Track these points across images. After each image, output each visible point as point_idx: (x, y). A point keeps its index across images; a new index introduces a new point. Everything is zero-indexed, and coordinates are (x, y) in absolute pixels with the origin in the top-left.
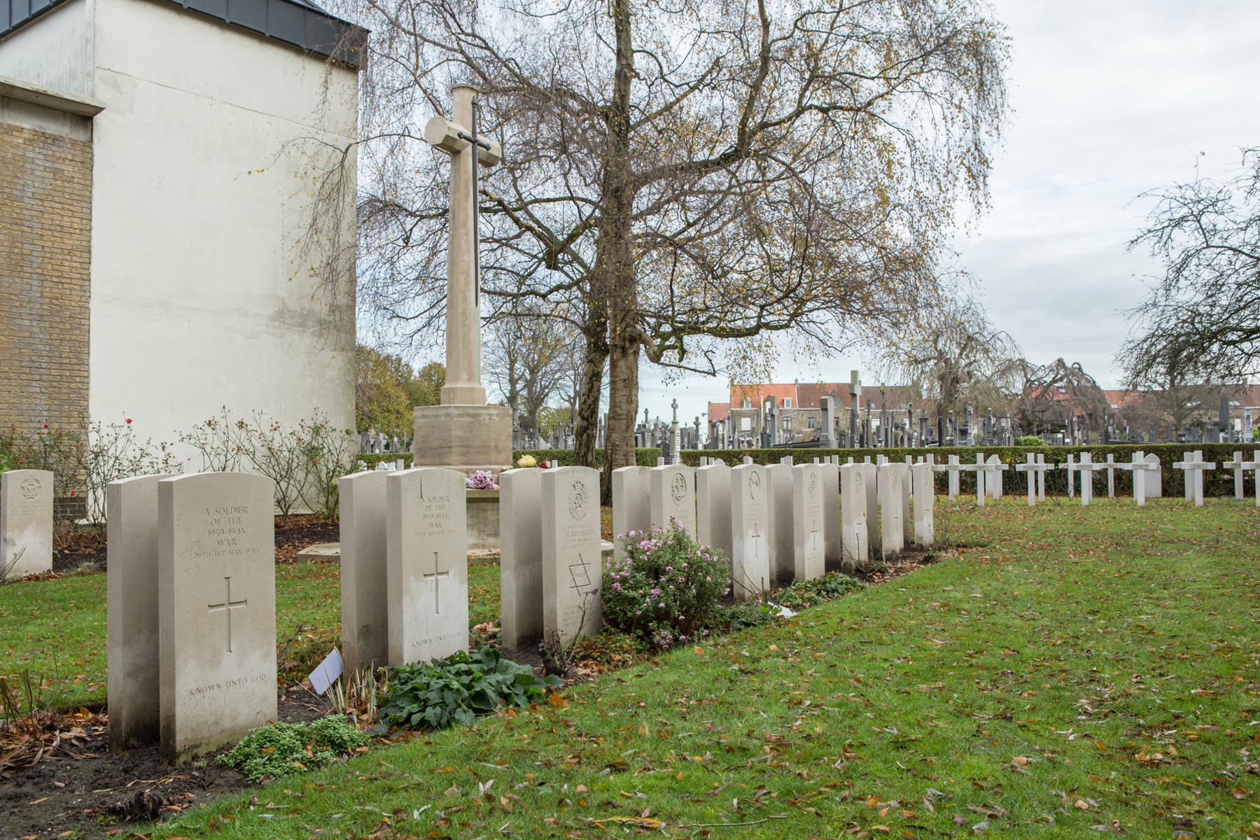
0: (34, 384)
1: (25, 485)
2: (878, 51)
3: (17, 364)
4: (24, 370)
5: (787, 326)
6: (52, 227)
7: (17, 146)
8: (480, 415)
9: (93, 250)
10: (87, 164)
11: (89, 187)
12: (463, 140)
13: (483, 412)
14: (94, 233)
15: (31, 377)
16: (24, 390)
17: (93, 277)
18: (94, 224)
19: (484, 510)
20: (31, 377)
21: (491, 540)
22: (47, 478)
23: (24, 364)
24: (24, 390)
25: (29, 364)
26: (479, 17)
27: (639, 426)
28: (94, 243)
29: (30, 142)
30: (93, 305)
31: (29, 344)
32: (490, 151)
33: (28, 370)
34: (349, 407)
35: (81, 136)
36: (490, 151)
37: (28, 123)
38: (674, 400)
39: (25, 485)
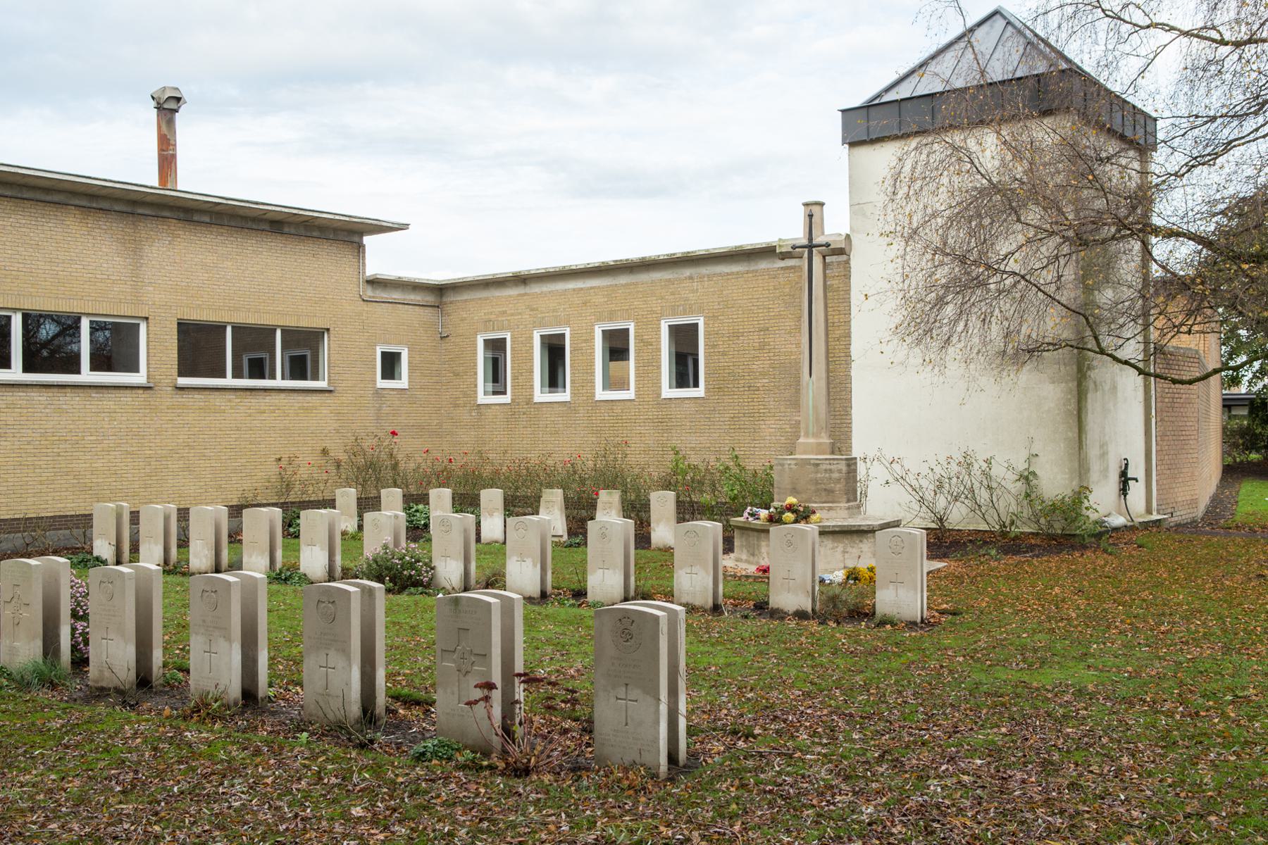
10: (847, 276)
12: (797, 250)
28: (853, 330)
34: (1070, 434)
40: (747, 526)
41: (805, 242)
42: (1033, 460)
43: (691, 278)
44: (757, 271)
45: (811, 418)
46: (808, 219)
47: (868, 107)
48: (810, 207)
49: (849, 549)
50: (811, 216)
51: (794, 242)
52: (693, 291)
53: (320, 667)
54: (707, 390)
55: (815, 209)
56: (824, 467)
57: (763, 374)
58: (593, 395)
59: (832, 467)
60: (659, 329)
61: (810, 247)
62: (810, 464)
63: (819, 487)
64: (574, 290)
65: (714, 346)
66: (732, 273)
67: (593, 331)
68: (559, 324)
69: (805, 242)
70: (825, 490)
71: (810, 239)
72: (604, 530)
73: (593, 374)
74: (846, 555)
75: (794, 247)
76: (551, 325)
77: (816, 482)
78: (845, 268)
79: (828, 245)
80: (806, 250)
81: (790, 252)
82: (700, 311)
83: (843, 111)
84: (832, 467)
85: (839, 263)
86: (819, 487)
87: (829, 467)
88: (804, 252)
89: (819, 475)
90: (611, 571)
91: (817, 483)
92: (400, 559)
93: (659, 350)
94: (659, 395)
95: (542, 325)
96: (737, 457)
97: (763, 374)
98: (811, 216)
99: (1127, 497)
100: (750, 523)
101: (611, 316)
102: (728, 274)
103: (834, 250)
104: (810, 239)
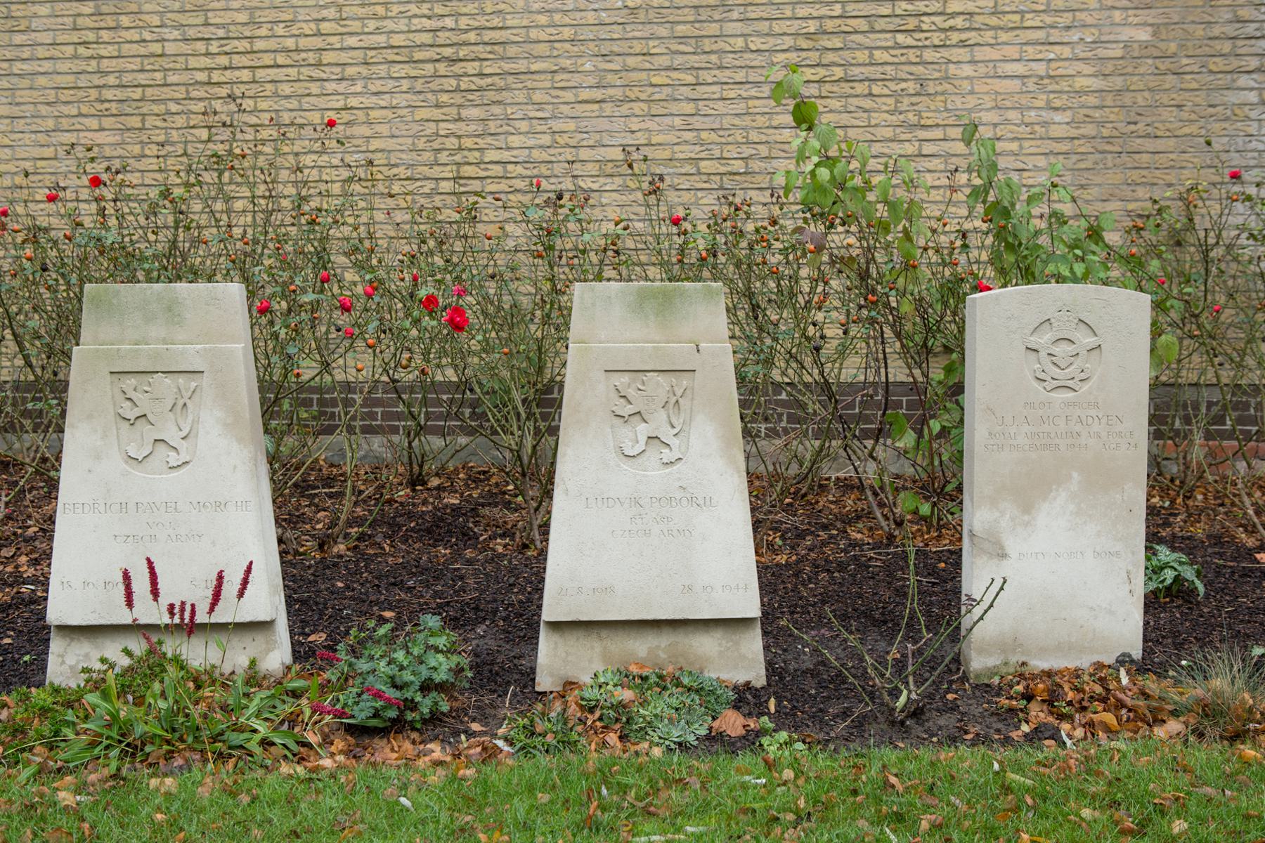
0: (1243, 81)
1: (1043, 340)
2: (227, 277)
3: (1200, 31)
4: (1218, 45)
5: (900, 156)
6: (458, 99)
15: (1235, 63)
16: (1216, 98)
20: (1235, 63)
22: (236, 290)
23: (1216, 31)
24: (1216, 98)
25: (1230, 30)
26: (387, 752)
33: (1226, 47)
38: (251, 563)
39: (1043, 340)
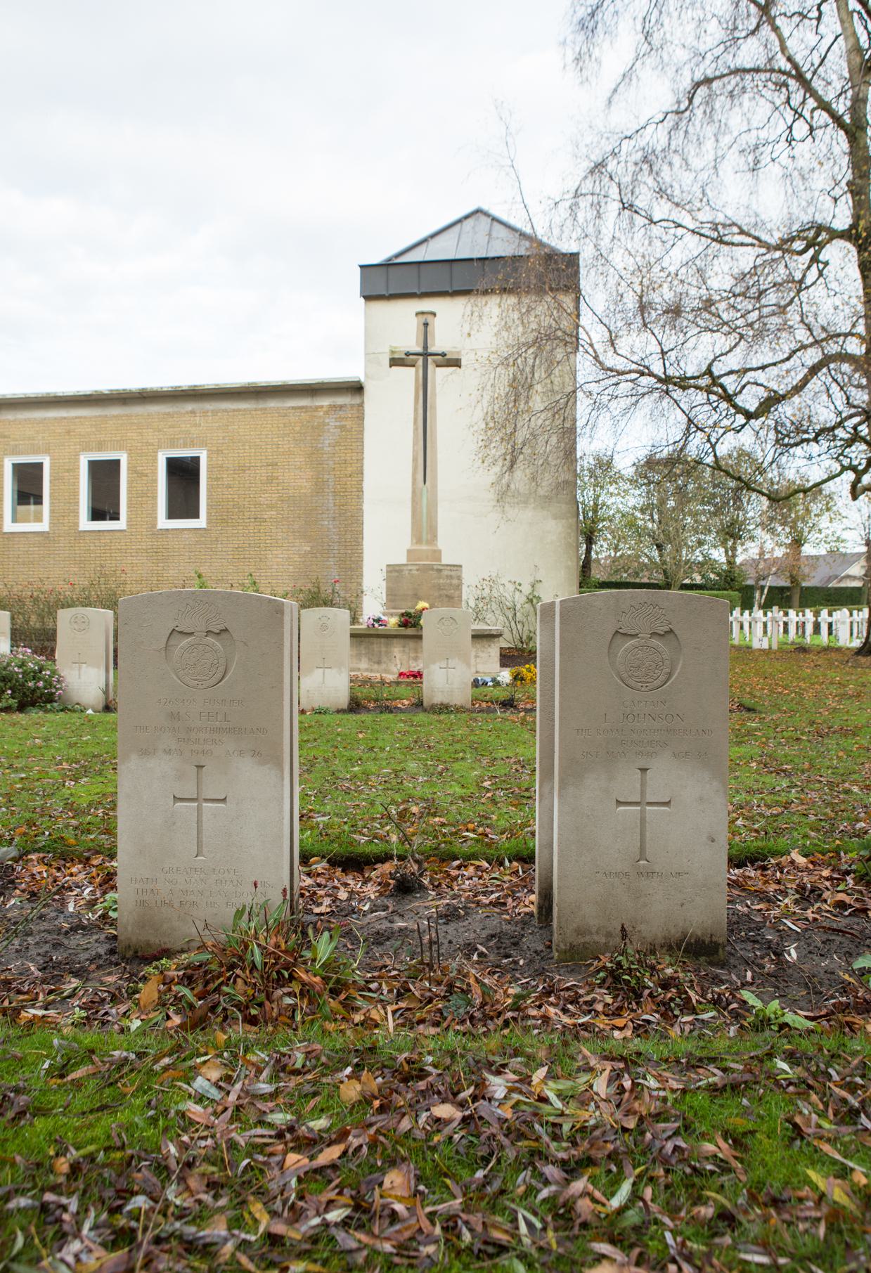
7: (320, 417)
8: (402, 571)
9: (365, 472)
10: (360, 418)
11: (361, 432)
12: (411, 357)
13: (405, 568)
14: (365, 462)
17: (364, 490)
18: (365, 455)
19: (373, 643)
21: (376, 666)
27: (394, 572)
28: (365, 467)
29: (327, 413)
30: (365, 507)
31: (327, 536)
32: (447, 357)
34: (570, 563)
35: (357, 400)
36: (447, 357)
37: (325, 402)
40: (371, 632)
41: (431, 350)
42: (538, 585)
43: (193, 412)
44: (266, 409)
45: (425, 524)
46: (422, 327)
47: (387, 265)
48: (425, 316)
49: (481, 654)
50: (426, 325)
51: (408, 349)
52: (195, 425)
53: (176, 799)
54: (209, 520)
55: (430, 318)
56: (446, 573)
57: (271, 507)
58: (77, 524)
59: (453, 573)
60: (155, 460)
61: (426, 354)
62: (433, 569)
63: (441, 592)
64: (56, 419)
65: (217, 479)
66: (239, 410)
67: (77, 461)
68: (36, 451)
69: (419, 349)
70: (447, 596)
71: (426, 347)
72: (324, 620)
73: (77, 503)
74: (478, 660)
75: (408, 354)
76: (27, 453)
77: (439, 588)
78: (358, 410)
79: (444, 355)
80: (421, 358)
81: (403, 359)
82: (203, 444)
83: (361, 267)
84: (453, 573)
85: (352, 406)
86: (441, 592)
87: (450, 573)
88: (416, 361)
89: (441, 581)
90: (334, 671)
91: (440, 589)
92: (20, 667)
93: (155, 481)
94: (155, 525)
95: (15, 452)
96: (255, 583)
97: (271, 507)
98: (426, 325)
99: (103, 685)
100: (377, 630)
101: (100, 447)
102: (234, 410)
103: (449, 360)
104: (426, 347)
